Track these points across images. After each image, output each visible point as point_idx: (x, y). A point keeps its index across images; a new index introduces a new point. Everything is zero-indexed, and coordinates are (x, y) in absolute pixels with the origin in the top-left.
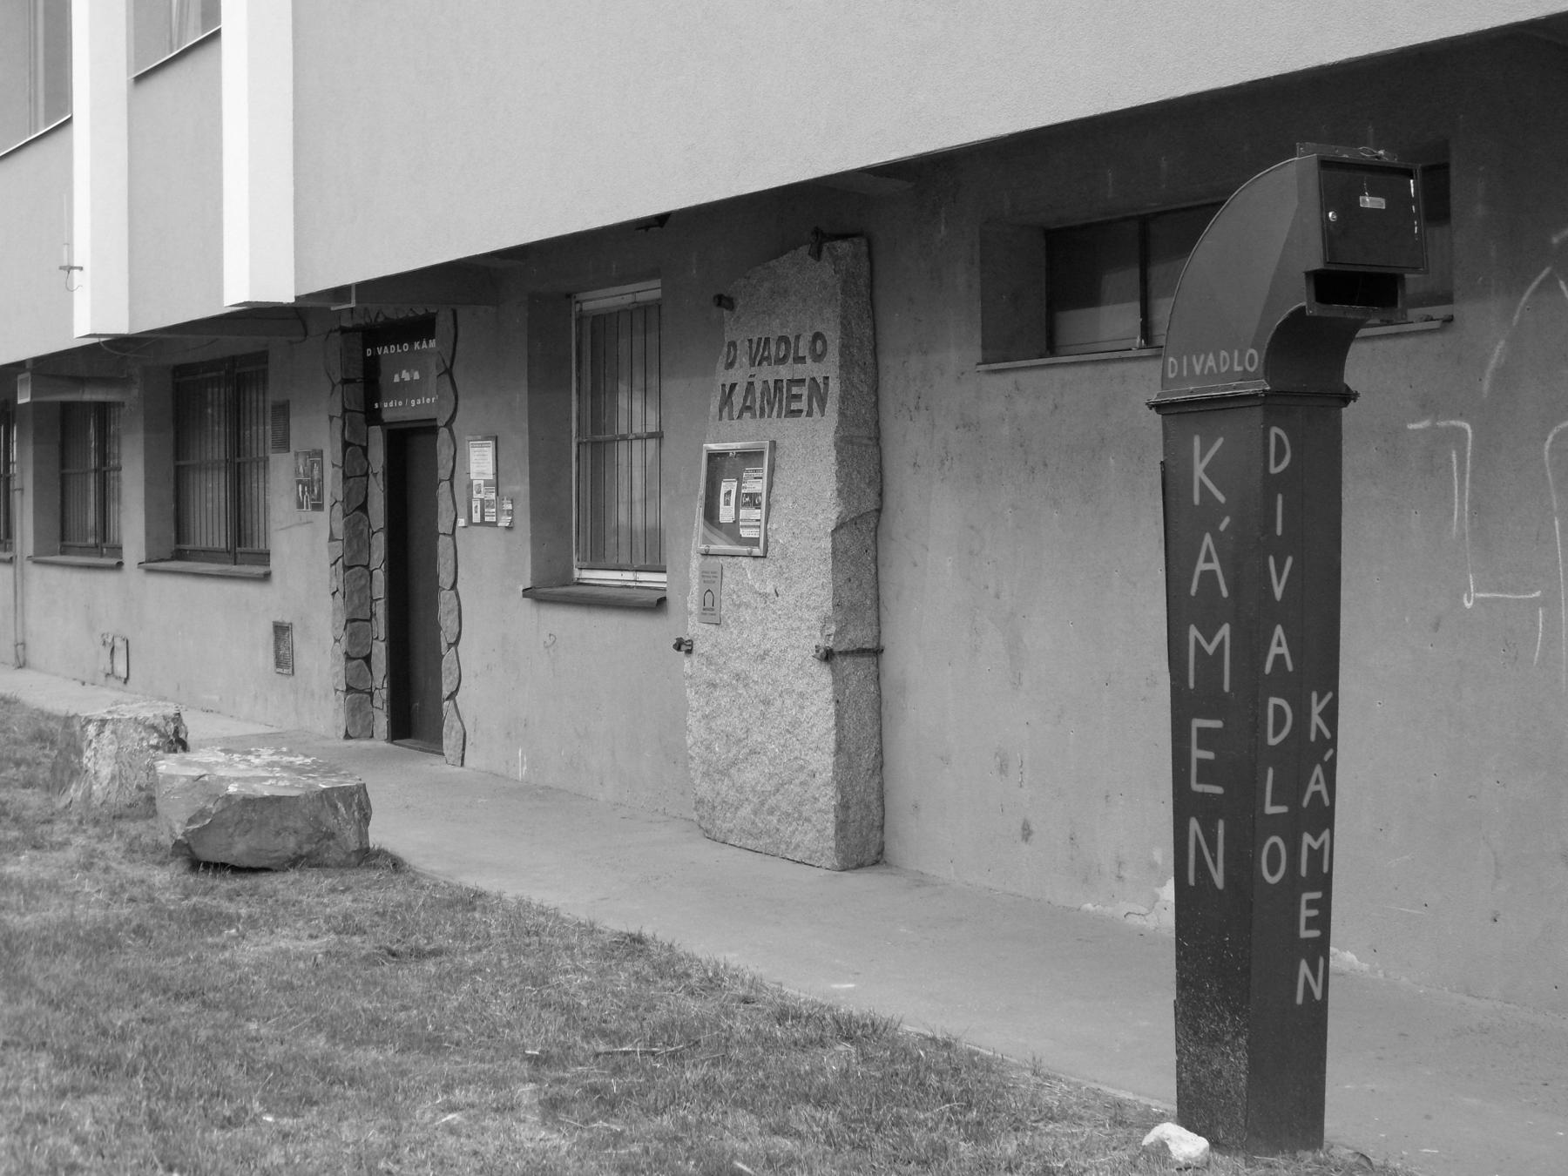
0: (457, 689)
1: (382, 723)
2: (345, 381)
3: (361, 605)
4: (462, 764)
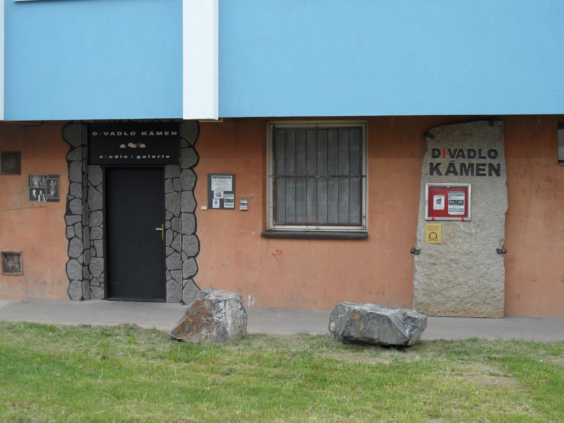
0: (195, 275)
1: (101, 292)
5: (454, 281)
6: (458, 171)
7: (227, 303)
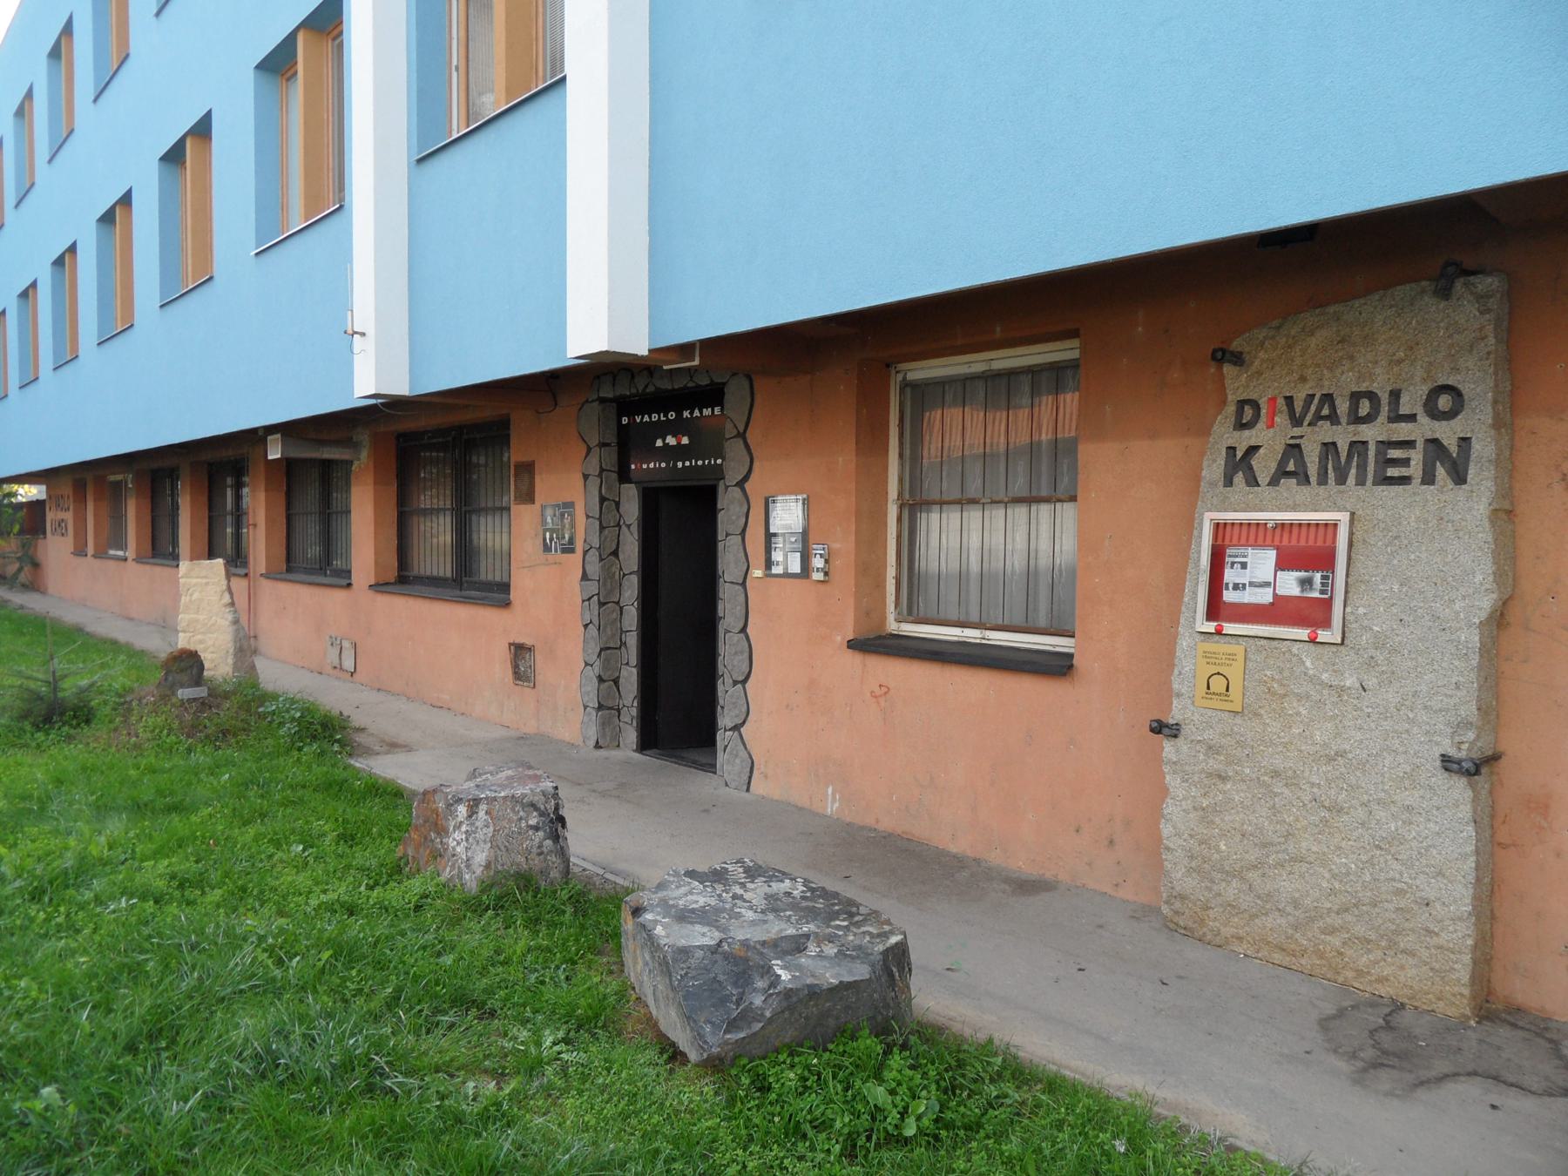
0: (744, 722)
1: (631, 736)
2: (603, 445)
3: (613, 635)
4: (748, 790)
5: (1283, 847)
6: (1313, 470)
7: (483, 807)
